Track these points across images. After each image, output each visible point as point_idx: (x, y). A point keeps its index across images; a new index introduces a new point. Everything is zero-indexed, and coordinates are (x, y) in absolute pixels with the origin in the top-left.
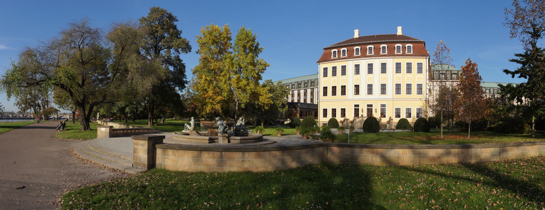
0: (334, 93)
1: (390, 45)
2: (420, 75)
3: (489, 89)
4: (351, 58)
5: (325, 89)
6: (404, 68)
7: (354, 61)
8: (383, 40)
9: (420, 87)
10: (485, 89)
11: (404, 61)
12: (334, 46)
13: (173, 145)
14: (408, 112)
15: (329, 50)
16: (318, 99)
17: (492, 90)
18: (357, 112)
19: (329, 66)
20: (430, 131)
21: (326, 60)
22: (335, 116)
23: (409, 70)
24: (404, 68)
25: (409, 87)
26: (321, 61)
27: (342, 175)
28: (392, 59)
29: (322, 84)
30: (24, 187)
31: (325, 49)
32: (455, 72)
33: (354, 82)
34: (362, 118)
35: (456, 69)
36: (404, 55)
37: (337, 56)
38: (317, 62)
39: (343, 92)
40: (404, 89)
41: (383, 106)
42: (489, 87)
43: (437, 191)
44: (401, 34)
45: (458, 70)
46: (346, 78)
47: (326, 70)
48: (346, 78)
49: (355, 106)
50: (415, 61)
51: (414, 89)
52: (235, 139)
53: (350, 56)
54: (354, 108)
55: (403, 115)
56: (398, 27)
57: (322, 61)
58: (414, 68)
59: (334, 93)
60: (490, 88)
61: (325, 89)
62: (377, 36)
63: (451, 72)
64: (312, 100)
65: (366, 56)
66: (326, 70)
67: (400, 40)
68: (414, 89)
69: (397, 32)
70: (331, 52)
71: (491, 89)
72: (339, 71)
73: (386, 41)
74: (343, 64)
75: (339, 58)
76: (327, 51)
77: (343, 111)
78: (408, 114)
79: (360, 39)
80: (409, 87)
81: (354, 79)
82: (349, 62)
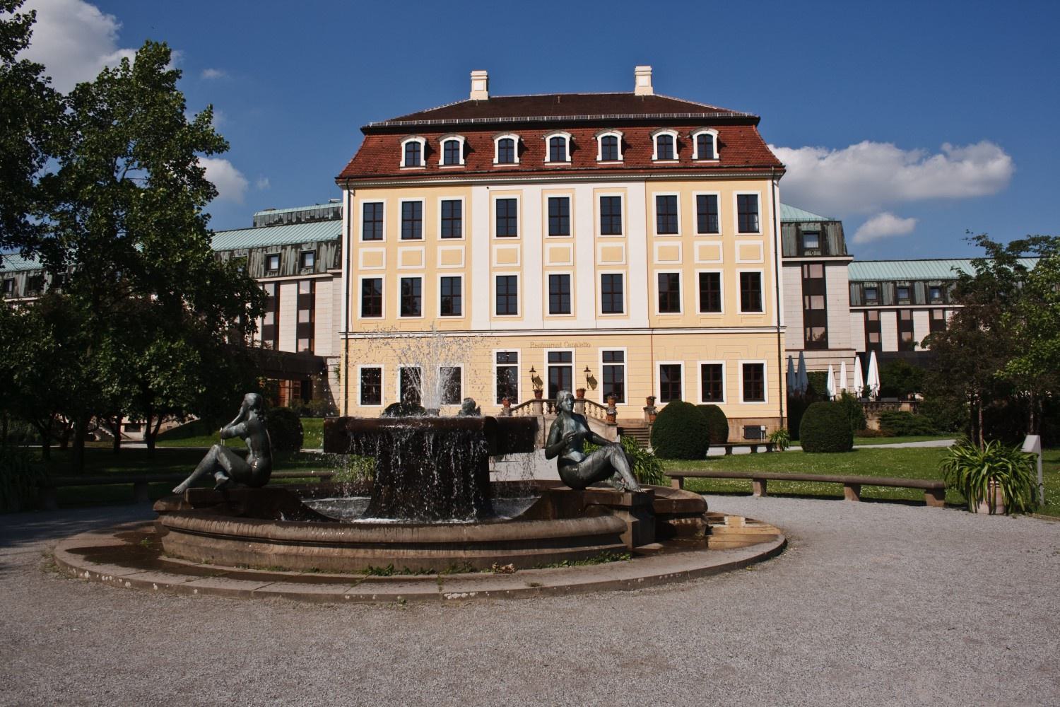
0: (410, 305)
2: (749, 240)
3: (907, 284)
4: (482, 175)
5: (372, 292)
6: (687, 214)
7: (492, 188)
8: (586, 114)
9: (751, 284)
10: (891, 285)
11: (687, 194)
12: (408, 123)
13: (908, 450)
14: (611, 381)
15: (389, 139)
18: (752, 380)
19: (392, 200)
20: (854, 447)
21: (378, 173)
22: (718, 396)
24: (687, 214)
25: (710, 285)
26: (353, 173)
28: (643, 184)
29: (361, 267)
30: (784, 546)
31: (367, 131)
32: (812, 228)
33: (547, 263)
34: (537, 405)
35: (813, 217)
38: (340, 179)
39: (451, 303)
40: (690, 293)
41: (613, 357)
42: (904, 277)
44: (483, 96)
45: (820, 218)
46: (462, 247)
47: (373, 215)
48: (462, 247)
49: (553, 357)
50: (727, 193)
51: (731, 293)
52: (29, 552)
53: (478, 167)
54: (495, 365)
55: (692, 392)
58: (728, 214)
59: (410, 305)
61: (372, 292)
62: (562, 96)
63: (798, 231)
64: (306, 331)
65: (542, 171)
66: (373, 215)
67: (668, 115)
68: (731, 293)
69: (469, 89)
71: (916, 284)
72: (432, 220)
73: (612, 116)
76: (376, 139)
78: (611, 386)
79: (492, 105)
80: (710, 285)
81: (572, 260)
82: (474, 189)
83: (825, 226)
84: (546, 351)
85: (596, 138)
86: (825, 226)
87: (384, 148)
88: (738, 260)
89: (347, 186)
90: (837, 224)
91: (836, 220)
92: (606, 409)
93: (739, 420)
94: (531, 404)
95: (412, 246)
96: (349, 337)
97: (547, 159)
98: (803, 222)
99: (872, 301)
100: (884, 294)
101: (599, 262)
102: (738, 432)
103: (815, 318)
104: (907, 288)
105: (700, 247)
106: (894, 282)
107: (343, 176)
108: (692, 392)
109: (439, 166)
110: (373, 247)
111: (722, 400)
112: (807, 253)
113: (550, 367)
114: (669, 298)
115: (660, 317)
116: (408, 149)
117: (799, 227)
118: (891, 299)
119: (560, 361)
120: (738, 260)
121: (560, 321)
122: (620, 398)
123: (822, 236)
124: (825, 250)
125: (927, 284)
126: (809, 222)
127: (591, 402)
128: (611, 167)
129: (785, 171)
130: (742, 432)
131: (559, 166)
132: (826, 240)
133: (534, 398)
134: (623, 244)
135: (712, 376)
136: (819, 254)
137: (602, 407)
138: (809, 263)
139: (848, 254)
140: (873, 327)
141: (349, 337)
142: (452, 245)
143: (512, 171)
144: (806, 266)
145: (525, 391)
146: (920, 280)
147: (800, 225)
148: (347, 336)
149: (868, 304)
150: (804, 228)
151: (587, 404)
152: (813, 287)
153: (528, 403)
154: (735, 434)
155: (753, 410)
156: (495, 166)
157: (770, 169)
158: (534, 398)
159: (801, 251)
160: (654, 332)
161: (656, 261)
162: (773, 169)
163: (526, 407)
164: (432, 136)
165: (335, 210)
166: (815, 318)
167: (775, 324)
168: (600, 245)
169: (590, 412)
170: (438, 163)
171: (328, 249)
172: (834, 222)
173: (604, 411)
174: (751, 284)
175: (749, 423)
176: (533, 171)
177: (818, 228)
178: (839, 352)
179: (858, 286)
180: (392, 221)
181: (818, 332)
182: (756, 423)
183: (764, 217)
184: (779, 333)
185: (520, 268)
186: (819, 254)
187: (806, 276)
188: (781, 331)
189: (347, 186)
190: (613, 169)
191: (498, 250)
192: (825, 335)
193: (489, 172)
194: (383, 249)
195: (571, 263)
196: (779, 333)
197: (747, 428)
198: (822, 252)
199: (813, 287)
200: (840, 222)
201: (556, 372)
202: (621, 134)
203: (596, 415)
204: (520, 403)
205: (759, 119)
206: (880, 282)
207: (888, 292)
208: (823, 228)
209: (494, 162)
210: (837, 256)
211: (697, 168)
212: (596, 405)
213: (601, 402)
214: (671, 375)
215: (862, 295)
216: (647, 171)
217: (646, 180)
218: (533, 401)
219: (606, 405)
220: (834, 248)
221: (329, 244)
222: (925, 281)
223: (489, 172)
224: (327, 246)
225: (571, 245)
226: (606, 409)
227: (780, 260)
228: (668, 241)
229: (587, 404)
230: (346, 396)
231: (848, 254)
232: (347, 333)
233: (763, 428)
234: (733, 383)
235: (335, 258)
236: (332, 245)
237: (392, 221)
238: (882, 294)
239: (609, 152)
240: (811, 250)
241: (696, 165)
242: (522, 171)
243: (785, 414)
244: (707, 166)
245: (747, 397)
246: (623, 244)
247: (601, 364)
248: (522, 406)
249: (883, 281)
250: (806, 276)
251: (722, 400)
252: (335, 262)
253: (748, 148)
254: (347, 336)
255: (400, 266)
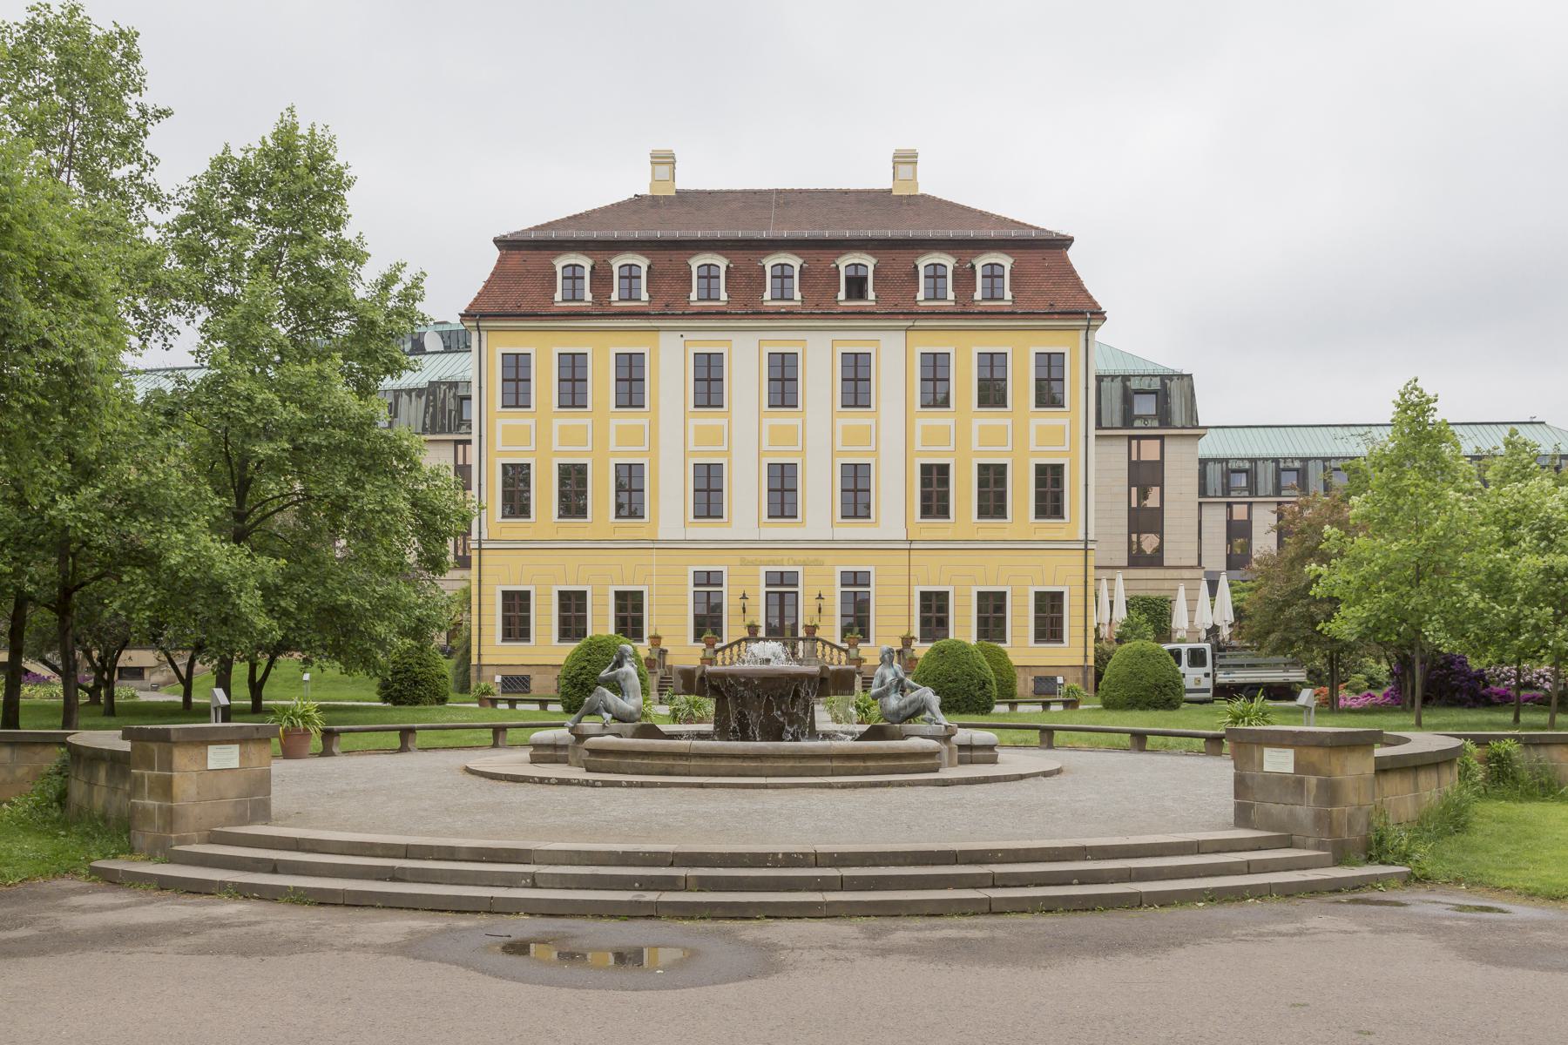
1: (663, 256)
2: (1050, 418)
3: (1297, 464)
4: (674, 316)
7: (688, 336)
10: (1271, 466)
15: (534, 259)
16: (480, 520)
17: (1316, 476)
21: (522, 310)
23: (992, 393)
24: (964, 381)
27: (171, 609)
29: (499, 447)
32: (1144, 384)
36: (965, 312)
37: (588, 296)
40: (964, 491)
41: (855, 579)
43: (226, 448)
47: (516, 375)
48: (645, 422)
51: (1021, 492)
55: (963, 627)
56: (1267, 768)
57: (496, 310)
60: (1305, 460)
63: (1125, 389)
66: (516, 375)
68: (1021, 492)
70: (554, 267)
71: (1311, 464)
72: (602, 380)
74: (629, 344)
75: (602, 312)
76: (517, 257)
77: (629, 609)
82: (663, 336)
83: (1168, 381)
84: (763, 570)
85: (837, 267)
86: (1168, 381)
87: (528, 271)
88: (1033, 447)
89: (478, 327)
90: (1185, 379)
91: (1184, 373)
92: (846, 651)
93: (1027, 669)
94: (743, 643)
95: (573, 418)
96: (483, 546)
97: (767, 296)
98: (1134, 376)
99: (1242, 489)
100: (1259, 480)
101: (839, 447)
102: (1026, 685)
103: (1145, 520)
104: (1297, 470)
105: (505, 427)
106: (1276, 460)
107: (472, 312)
108: (963, 627)
109: (610, 302)
110: (516, 418)
111: (1005, 642)
112: (1137, 423)
113: (767, 593)
114: (934, 499)
115: (980, 525)
116: (698, 391)
117: (1128, 383)
118: (1270, 487)
119: (782, 588)
120: (1033, 447)
121: (782, 530)
122: (865, 636)
123: (1162, 396)
124: (1164, 417)
125: (1327, 464)
126: (1143, 376)
127: (825, 643)
128: (700, 310)
129: (1105, 319)
130: (1031, 685)
131: (783, 307)
132: (1167, 403)
133: (747, 635)
134: (799, 422)
135: (992, 609)
136: (1156, 423)
137: (840, 649)
138: (1139, 438)
139: (1200, 425)
140: (1238, 531)
141: (483, 546)
142: (630, 418)
143: (718, 313)
144: (1134, 443)
145: (732, 629)
146: (1316, 458)
147: (1129, 380)
148: (480, 544)
149: (1233, 494)
150: (1134, 384)
151: (819, 643)
152: (1145, 476)
153: (738, 642)
154: (1024, 686)
155: (515, 655)
156: (692, 304)
157: (1084, 316)
158: (747, 635)
159: (1128, 419)
160: (913, 546)
161: (918, 446)
162: (1089, 316)
163: (728, 650)
164: (600, 256)
165: (416, 337)
166: (1145, 520)
167: (1082, 537)
168: (840, 423)
169: (824, 656)
170: (610, 297)
171: (411, 401)
172: (1181, 376)
173: (843, 653)
174: (1050, 482)
175: (1041, 673)
176: (747, 314)
177: (1156, 384)
178: (1179, 571)
179: (1218, 466)
180: (545, 381)
181: (1149, 542)
182: (1051, 673)
183: (1075, 388)
184: (1086, 549)
185: (728, 453)
186: (1156, 423)
187: (1134, 458)
188: (1089, 546)
189: (478, 327)
190: (860, 313)
191: (696, 426)
192: (1160, 550)
193: (753, 314)
194: (531, 422)
195: (799, 448)
196: (1086, 549)
197: (1038, 680)
198: (1160, 421)
199: (1145, 476)
200: (1190, 376)
201: (775, 599)
202: (874, 261)
203: (824, 656)
204: (725, 643)
205: (1071, 240)
206: (1253, 460)
207: (1266, 476)
208: (1164, 385)
209: (612, 299)
210: (1183, 428)
211: (981, 313)
212: (833, 646)
213: (838, 642)
214: (934, 608)
215: (1225, 481)
216: (909, 317)
217: (907, 329)
218: (745, 640)
219: (846, 646)
220: (1178, 416)
221: (413, 394)
222: (1325, 459)
223: (684, 314)
224: (410, 397)
225: (799, 422)
226: (846, 651)
227: (1092, 432)
228: (937, 419)
229: (819, 643)
230: (1086, 582)
231: (1200, 425)
232: (480, 540)
233: (1060, 680)
234: (1021, 619)
235: (425, 417)
236: (419, 396)
237: (545, 381)
238: (1256, 478)
239: (856, 286)
240: (1144, 417)
241: (980, 309)
242: (730, 314)
243: (1091, 662)
244: (994, 310)
245: (1041, 636)
246: (872, 422)
247: (838, 589)
248: (730, 646)
249: (1259, 459)
250: (1134, 458)
251: (1005, 642)
252: (424, 423)
253: (1054, 284)
254: (480, 544)
255: (555, 446)
